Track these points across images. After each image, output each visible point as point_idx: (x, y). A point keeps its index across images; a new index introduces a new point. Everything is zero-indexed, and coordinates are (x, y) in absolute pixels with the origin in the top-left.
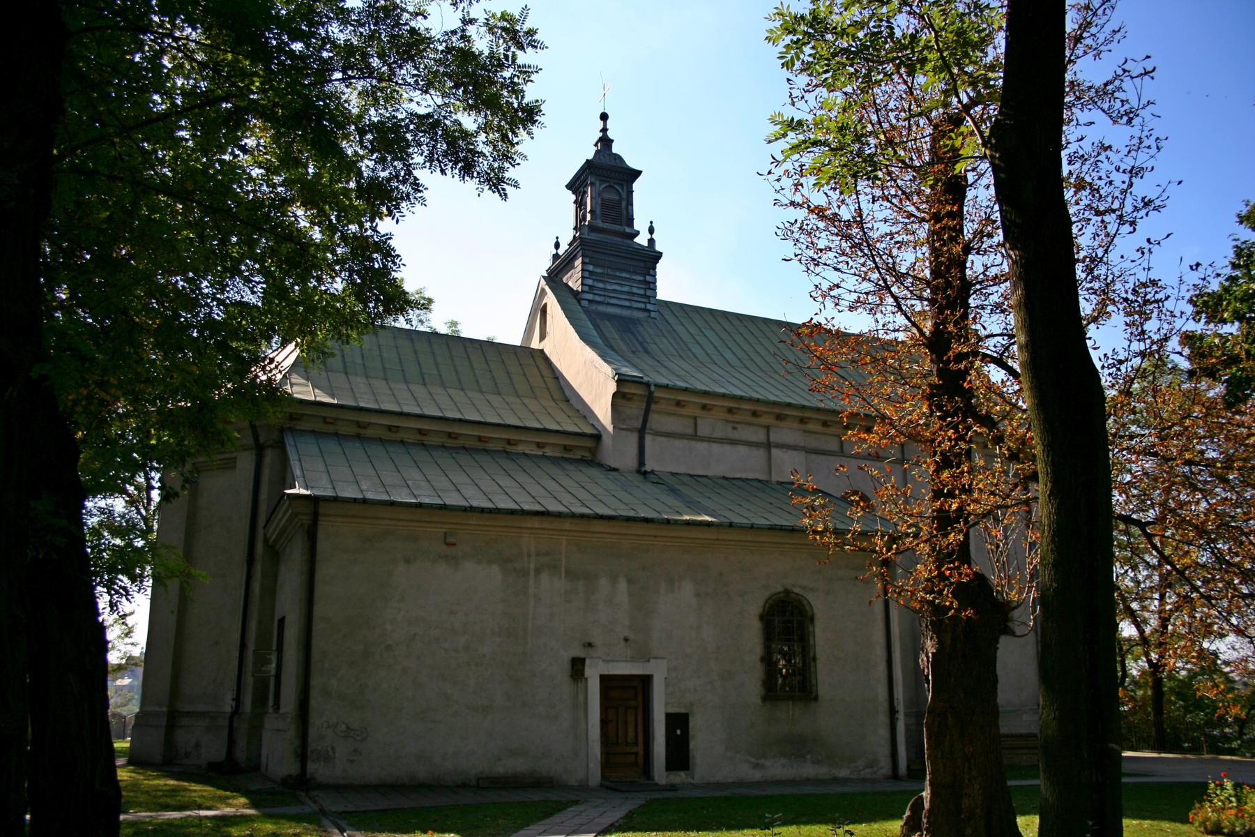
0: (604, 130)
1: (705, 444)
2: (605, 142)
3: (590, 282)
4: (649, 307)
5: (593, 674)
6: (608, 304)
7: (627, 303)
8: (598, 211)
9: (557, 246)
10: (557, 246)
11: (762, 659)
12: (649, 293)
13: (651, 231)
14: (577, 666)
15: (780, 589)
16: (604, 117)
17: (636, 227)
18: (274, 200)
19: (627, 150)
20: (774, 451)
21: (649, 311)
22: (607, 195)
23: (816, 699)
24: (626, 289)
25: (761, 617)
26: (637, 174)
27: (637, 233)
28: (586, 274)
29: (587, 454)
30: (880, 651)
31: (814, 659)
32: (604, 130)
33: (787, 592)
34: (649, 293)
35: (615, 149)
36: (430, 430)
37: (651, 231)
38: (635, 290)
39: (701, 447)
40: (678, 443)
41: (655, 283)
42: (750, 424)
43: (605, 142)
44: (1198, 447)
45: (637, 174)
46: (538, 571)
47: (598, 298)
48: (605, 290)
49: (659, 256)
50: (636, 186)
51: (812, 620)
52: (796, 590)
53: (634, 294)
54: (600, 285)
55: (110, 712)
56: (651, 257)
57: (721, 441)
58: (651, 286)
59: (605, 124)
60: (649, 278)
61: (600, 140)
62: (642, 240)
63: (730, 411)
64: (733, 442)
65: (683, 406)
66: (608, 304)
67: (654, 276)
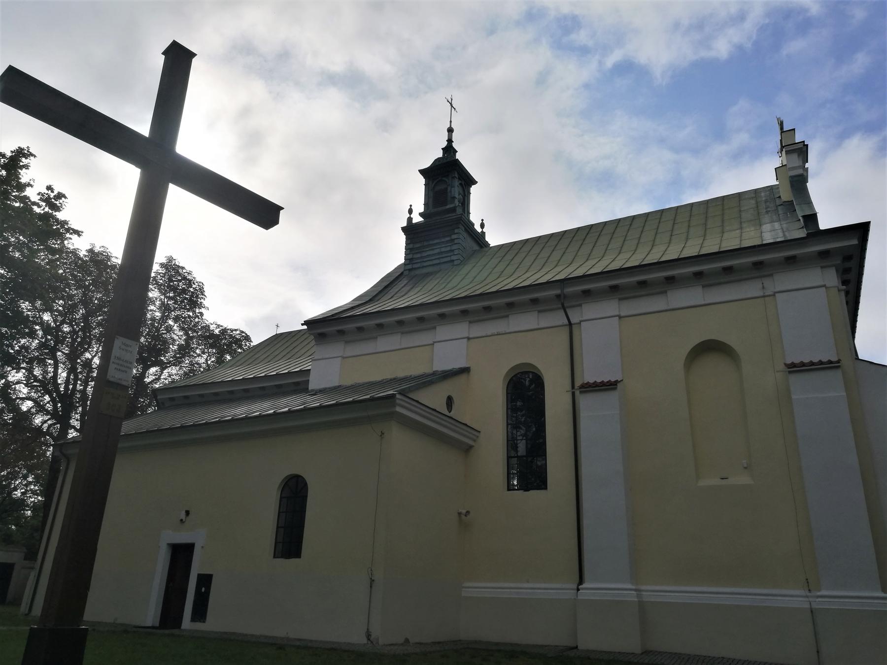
0: (450, 141)
2: (449, 150)
4: (454, 258)
6: (423, 267)
7: (437, 261)
9: (410, 211)
10: (410, 211)
13: (482, 226)
18: (174, 356)
26: (422, 172)
32: (450, 141)
37: (482, 226)
38: (443, 250)
43: (449, 150)
44: (171, 322)
45: (422, 172)
48: (422, 257)
54: (418, 255)
60: (411, 246)
66: (423, 267)
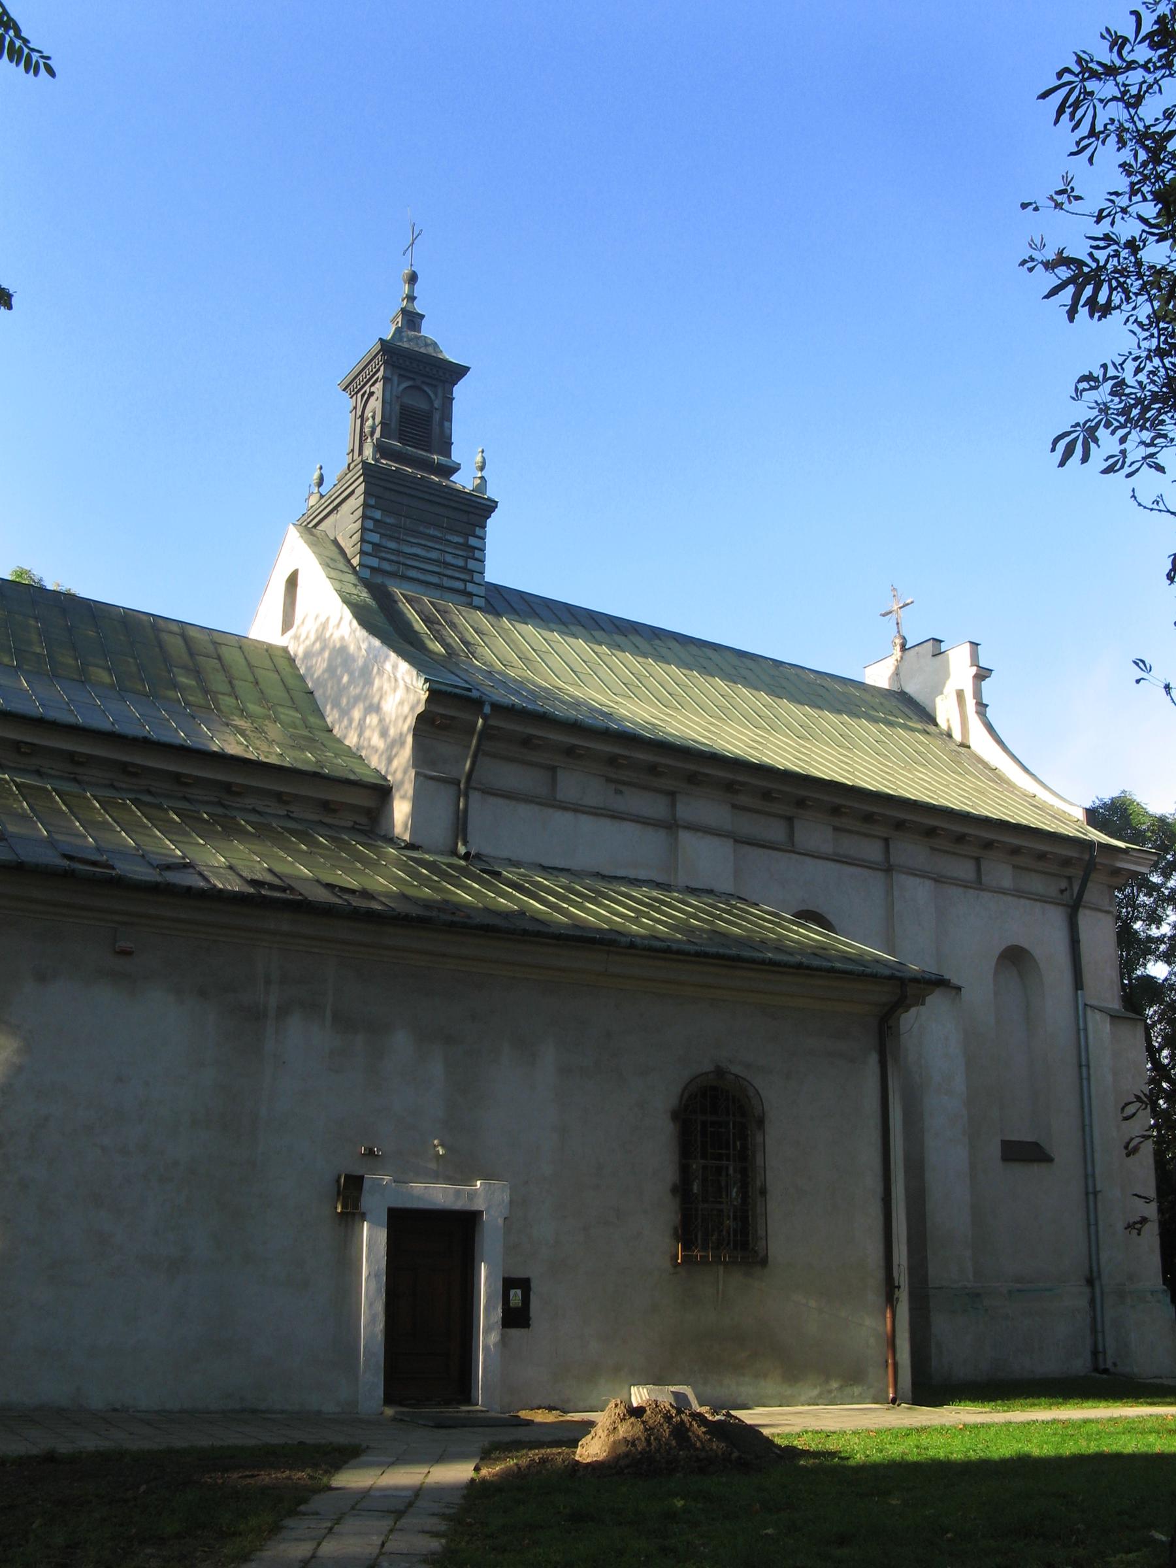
0: (411, 298)
1: (569, 816)
2: (412, 319)
3: (375, 538)
4: (470, 587)
5: (375, 1202)
7: (434, 579)
8: (394, 425)
11: (674, 1190)
12: (472, 564)
14: (350, 1189)
15: (708, 1067)
16: (413, 278)
17: (457, 455)
19: (446, 337)
20: (684, 836)
21: (470, 595)
22: (408, 400)
23: (764, 1262)
24: (434, 555)
25: (675, 1116)
26: (460, 372)
27: (455, 469)
28: (370, 524)
29: (363, 820)
30: (872, 1182)
31: (763, 1192)
32: (411, 298)
33: (720, 1072)
34: (472, 564)
35: (427, 330)
36: (90, 757)
38: (449, 559)
39: (563, 819)
40: (524, 810)
41: (483, 550)
42: (645, 788)
45: (460, 372)
46: (283, 1011)
47: (386, 566)
48: (398, 552)
49: (489, 507)
50: (460, 390)
51: (761, 1122)
52: (736, 1069)
53: (447, 565)
54: (392, 545)
55: (393, 655)
56: (478, 509)
57: (595, 812)
58: (475, 553)
59: (412, 289)
61: (404, 311)
62: (464, 480)
63: (612, 761)
64: (616, 816)
65: (334, 811)
67: (483, 538)
